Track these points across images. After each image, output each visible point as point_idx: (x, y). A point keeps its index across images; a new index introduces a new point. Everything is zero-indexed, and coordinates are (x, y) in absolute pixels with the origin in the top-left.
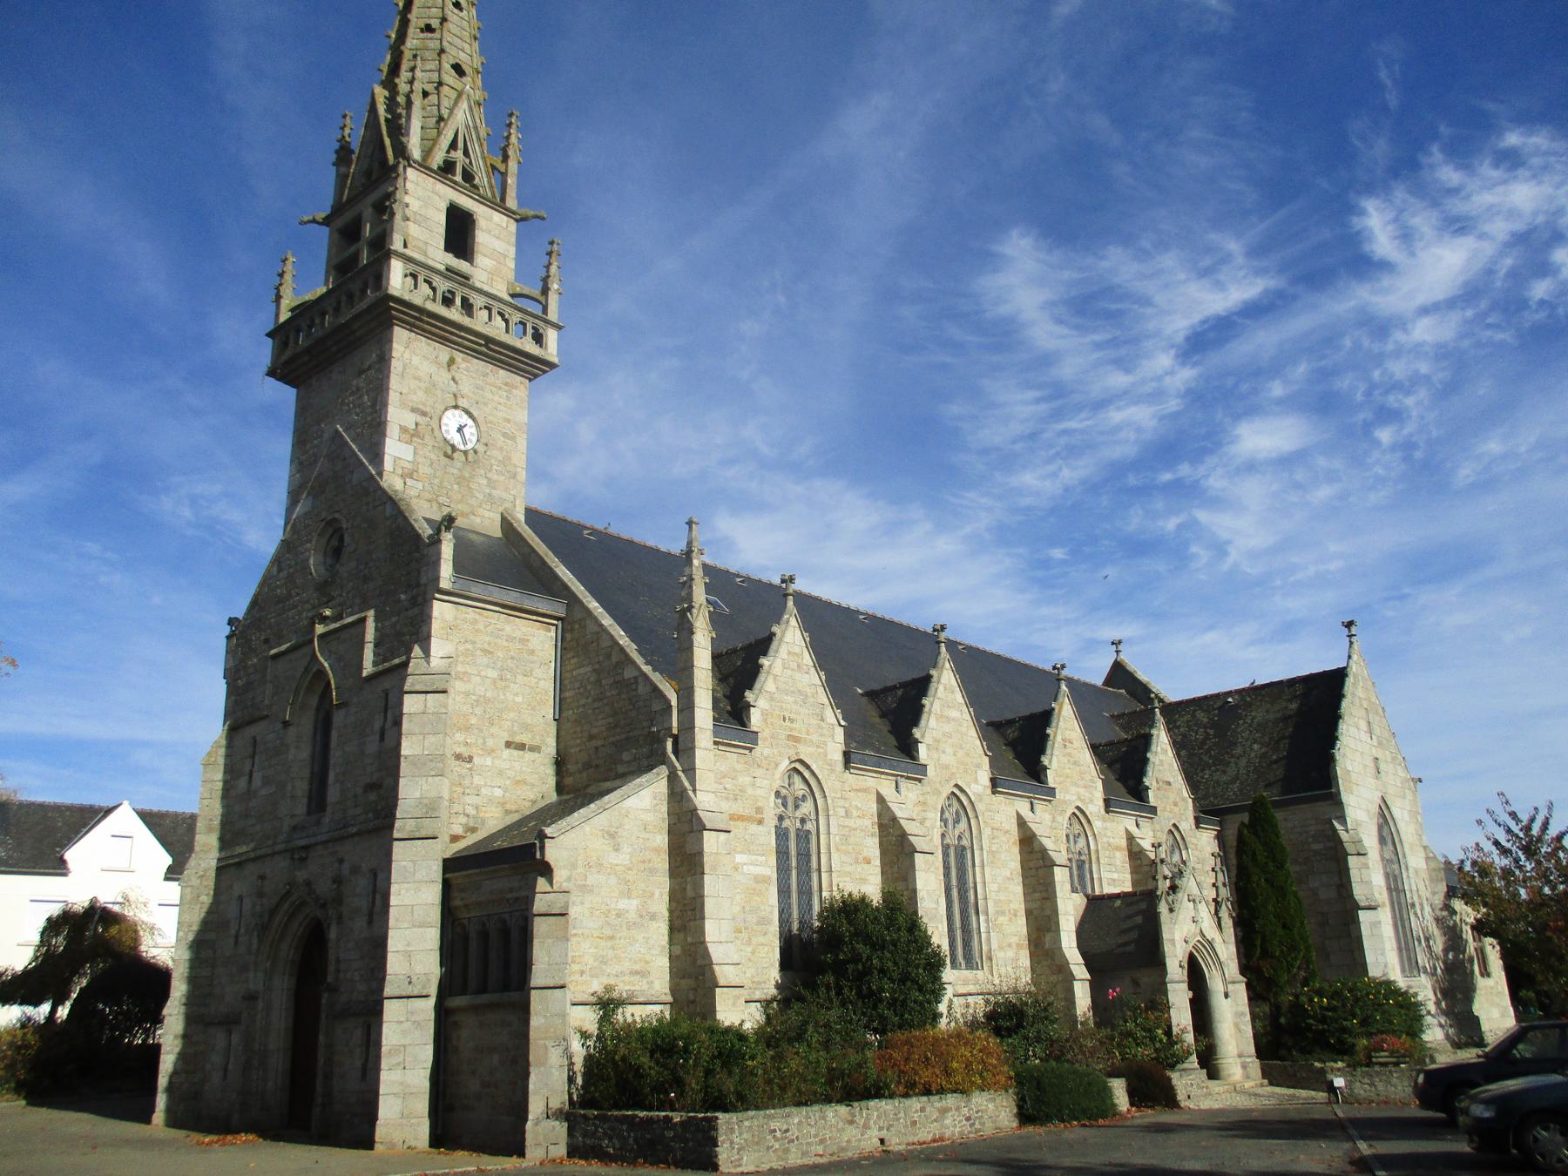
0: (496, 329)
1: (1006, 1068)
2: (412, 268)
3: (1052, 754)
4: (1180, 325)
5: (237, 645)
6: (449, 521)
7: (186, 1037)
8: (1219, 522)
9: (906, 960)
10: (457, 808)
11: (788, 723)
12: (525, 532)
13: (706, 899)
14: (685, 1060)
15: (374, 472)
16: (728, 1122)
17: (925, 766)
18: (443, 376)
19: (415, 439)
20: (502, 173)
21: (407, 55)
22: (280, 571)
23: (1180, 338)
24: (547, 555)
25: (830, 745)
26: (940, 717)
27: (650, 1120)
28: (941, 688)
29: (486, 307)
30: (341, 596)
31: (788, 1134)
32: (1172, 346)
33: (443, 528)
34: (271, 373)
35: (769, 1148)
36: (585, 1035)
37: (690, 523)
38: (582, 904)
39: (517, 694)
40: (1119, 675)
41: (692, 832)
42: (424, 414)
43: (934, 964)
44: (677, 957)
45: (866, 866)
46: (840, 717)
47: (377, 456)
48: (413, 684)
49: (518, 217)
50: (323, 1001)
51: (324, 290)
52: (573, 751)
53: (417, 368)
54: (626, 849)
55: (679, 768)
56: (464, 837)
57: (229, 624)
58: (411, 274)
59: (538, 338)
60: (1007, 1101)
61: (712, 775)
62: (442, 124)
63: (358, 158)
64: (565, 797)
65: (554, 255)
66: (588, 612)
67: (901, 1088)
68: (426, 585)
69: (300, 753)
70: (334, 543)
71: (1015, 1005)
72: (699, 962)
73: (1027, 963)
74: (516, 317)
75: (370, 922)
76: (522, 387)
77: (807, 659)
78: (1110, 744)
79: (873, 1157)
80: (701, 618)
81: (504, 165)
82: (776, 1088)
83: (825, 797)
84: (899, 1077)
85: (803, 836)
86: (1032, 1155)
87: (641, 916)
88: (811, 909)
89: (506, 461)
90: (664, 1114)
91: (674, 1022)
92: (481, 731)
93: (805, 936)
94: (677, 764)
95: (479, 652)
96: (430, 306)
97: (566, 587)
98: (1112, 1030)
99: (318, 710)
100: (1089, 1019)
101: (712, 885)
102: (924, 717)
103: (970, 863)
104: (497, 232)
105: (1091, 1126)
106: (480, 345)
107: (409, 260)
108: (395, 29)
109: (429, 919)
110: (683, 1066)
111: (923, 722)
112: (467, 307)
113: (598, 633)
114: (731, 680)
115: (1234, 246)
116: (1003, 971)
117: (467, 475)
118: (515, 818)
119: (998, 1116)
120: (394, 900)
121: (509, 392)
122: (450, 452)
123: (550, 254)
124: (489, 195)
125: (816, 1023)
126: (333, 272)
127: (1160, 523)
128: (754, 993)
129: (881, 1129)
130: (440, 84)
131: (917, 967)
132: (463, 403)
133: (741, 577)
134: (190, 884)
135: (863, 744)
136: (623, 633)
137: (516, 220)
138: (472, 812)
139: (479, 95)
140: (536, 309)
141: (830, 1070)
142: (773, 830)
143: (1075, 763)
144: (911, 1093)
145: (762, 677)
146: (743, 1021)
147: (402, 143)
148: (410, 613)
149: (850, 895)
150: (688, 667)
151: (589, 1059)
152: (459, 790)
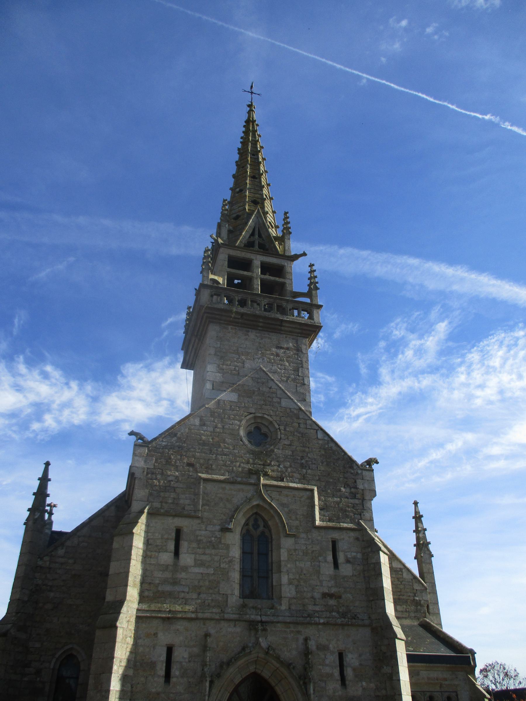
134: (122, 626)
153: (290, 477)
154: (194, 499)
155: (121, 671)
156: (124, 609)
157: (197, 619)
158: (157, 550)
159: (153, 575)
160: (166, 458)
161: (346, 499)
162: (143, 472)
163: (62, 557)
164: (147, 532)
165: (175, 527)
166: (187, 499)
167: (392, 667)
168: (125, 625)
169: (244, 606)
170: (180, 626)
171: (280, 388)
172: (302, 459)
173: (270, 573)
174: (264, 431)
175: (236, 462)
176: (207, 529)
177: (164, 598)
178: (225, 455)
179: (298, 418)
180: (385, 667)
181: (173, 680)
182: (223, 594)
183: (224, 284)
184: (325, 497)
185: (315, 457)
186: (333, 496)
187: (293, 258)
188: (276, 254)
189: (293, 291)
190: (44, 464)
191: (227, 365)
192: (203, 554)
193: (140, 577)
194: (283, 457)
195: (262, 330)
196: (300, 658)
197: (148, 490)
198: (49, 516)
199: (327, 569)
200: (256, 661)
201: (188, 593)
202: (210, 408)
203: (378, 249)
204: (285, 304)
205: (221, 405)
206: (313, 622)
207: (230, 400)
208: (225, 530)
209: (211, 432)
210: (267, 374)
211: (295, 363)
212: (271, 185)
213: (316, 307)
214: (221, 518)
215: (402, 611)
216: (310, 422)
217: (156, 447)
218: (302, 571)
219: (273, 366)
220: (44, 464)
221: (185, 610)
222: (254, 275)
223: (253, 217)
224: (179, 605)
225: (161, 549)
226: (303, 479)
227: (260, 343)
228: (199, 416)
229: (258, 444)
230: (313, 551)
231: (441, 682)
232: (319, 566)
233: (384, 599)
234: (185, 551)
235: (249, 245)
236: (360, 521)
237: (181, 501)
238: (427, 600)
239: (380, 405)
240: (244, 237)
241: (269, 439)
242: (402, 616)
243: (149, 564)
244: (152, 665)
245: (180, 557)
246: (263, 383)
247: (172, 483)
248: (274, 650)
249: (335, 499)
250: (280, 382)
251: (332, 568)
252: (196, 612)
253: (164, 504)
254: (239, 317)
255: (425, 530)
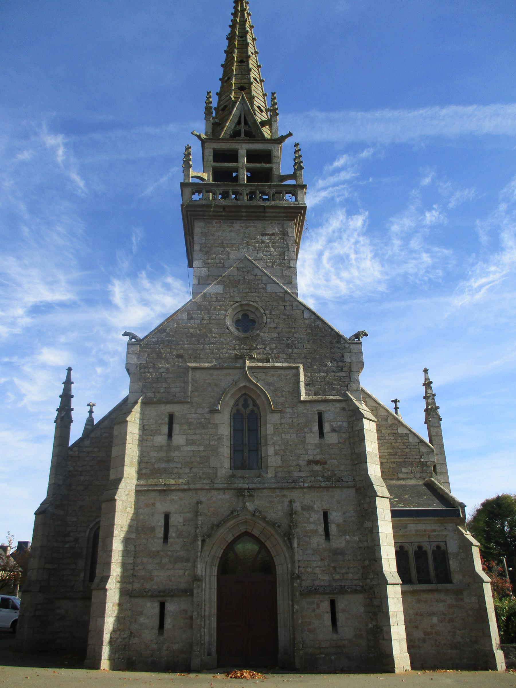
4: (31, 299)
8: (23, 386)
23: (30, 304)
37: (426, 371)
115: (62, 277)
134: (121, 499)
153: (276, 358)
154: (184, 387)
155: (122, 535)
156: (122, 485)
157: (189, 490)
158: (153, 434)
159: (149, 455)
160: (157, 353)
161: (333, 373)
162: (137, 367)
163: (88, 447)
164: (142, 419)
165: (168, 412)
166: (177, 387)
167: (373, 522)
168: (124, 498)
169: (233, 476)
170: (175, 496)
171: (265, 274)
172: (288, 340)
173: (259, 446)
174: (251, 318)
175: (223, 349)
176: (197, 412)
177: (160, 474)
178: (213, 344)
179: (284, 301)
180: (367, 522)
181: (170, 540)
182: (213, 467)
183: (209, 179)
184: (310, 372)
185: (302, 336)
186: (320, 371)
187: (279, 140)
188: (264, 140)
189: (281, 174)
190: (67, 369)
191: (212, 259)
192: (194, 434)
193: (137, 458)
194: (269, 339)
195: (246, 220)
196: (285, 518)
197: (142, 383)
198: (89, 414)
199: (313, 439)
200: (246, 522)
201: (181, 469)
202: (197, 302)
203: (484, 102)
204: (268, 189)
205: (207, 298)
206: (298, 486)
207: (215, 292)
208: (213, 411)
209: (198, 324)
210: (252, 262)
211: (281, 248)
212: (262, 66)
213: (299, 188)
214: (209, 401)
215: (407, 473)
216: (296, 303)
217: (147, 344)
218: (288, 442)
219: (258, 253)
220: (67, 369)
221: (178, 483)
222: (240, 165)
223: (237, 105)
224: (173, 479)
225: (157, 433)
226: (290, 358)
227: (245, 233)
228: (186, 311)
229: (245, 331)
230: (299, 424)
231: (430, 533)
232: (305, 437)
233: (366, 462)
234: (178, 433)
235: (235, 135)
236: (346, 392)
237: (173, 390)
238: (433, 461)
239: (504, 272)
240: (229, 127)
241: (256, 325)
242: (407, 477)
243: (145, 446)
244: (152, 529)
245: (173, 439)
246: (248, 271)
247: (163, 374)
248: (260, 512)
249: (322, 374)
250: (265, 268)
251: (318, 438)
252: (188, 483)
253: (156, 394)
254: (221, 210)
255: (434, 395)
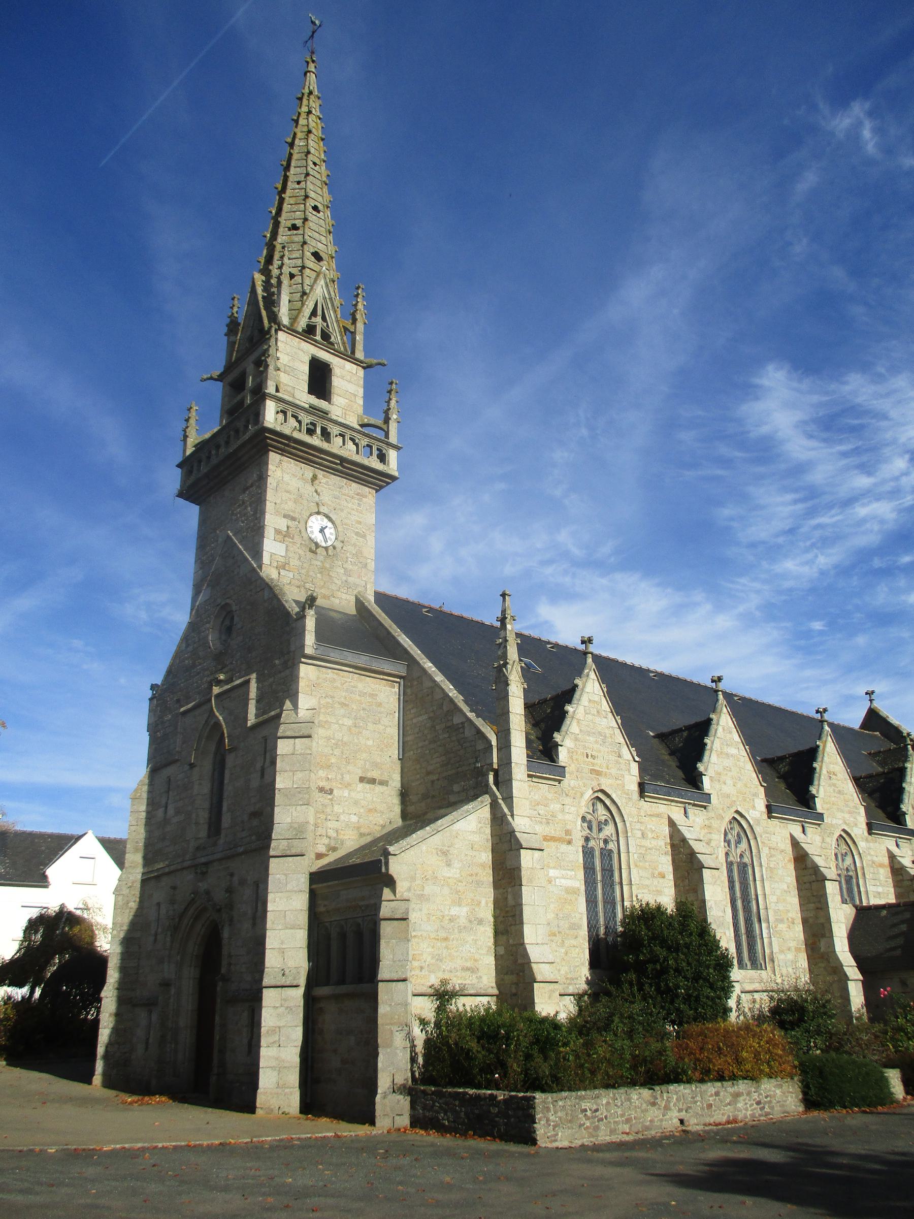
0: (349, 451)
1: (790, 1058)
2: (282, 406)
3: (819, 785)
5: (157, 706)
6: (311, 601)
7: (118, 1015)
9: (698, 961)
10: (320, 831)
11: (590, 759)
12: (374, 609)
13: (524, 908)
14: (508, 1045)
15: (255, 566)
16: (544, 1102)
17: (710, 795)
18: (309, 489)
19: (286, 539)
20: (352, 333)
21: (278, 247)
22: (188, 646)
24: (390, 627)
25: (627, 777)
26: (720, 754)
27: (478, 1097)
28: (720, 729)
29: (340, 435)
30: (232, 663)
31: (597, 1114)
32: (907, 452)
33: (307, 606)
34: (180, 495)
35: (581, 1125)
36: (423, 1022)
37: (504, 595)
38: (421, 910)
39: (368, 739)
40: (874, 719)
41: (511, 850)
42: (293, 519)
43: (723, 965)
44: (502, 956)
45: (661, 880)
46: (635, 754)
47: (257, 553)
48: (284, 731)
49: (365, 365)
50: (218, 989)
51: (219, 428)
52: (414, 784)
53: (288, 484)
54: (456, 864)
55: (499, 796)
56: (327, 855)
57: (151, 689)
58: (282, 411)
59: (382, 458)
60: (793, 1087)
61: (527, 803)
62: (305, 297)
63: (243, 328)
64: (408, 822)
65: (393, 392)
66: (424, 671)
67: (697, 1074)
68: (294, 652)
69: (202, 789)
70: (227, 623)
71: (796, 1001)
72: (520, 961)
73: (805, 964)
74: (364, 442)
75: (254, 924)
76: (370, 496)
77: (605, 706)
78: (870, 776)
79: (674, 1136)
80: (514, 672)
81: (353, 327)
82: (586, 1071)
83: (624, 821)
84: (695, 1064)
85: (607, 855)
86: (818, 1141)
87: (470, 921)
88: (615, 916)
89: (358, 554)
90: (489, 1092)
91: (499, 1012)
92: (339, 768)
93: (610, 939)
94: (498, 794)
95: (336, 705)
96: (296, 435)
97: (405, 650)
98: (885, 1025)
99: (216, 754)
100: (863, 1015)
101: (529, 895)
102: (707, 753)
103: (751, 878)
104: (349, 378)
105: (871, 1113)
106: (336, 464)
107: (280, 400)
108: (270, 230)
109: (299, 923)
110: (506, 1050)
111: (706, 758)
112: (326, 434)
113: (432, 687)
114: (543, 725)
116: (784, 972)
117: (328, 566)
118: (369, 839)
119: (785, 1101)
120: (270, 907)
121: (360, 500)
122: (314, 548)
123: (390, 392)
124: (342, 349)
125: (622, 1016)
126: (226, 416)
127: (903, 598)
128: (568, 988)
129: (680, 1110)
130: (303, 267)
131: (708, 967)
132: (323, 509)
133: (551, 644)
134: (121, 893)
135: (655, 777)
136: (451, 687)
137: (363, 368)
138: (332, 833)
139: (333, 274)
140: (380, 435)
141: (634, 1057)
142: (580, 849)
143: (839, 792)
144: (706, 1078)
145: (567, 721)
146: (557, 1012)
147: (274, 312)
148: (283, 674)
149: (648, 904)
150: (506, 713)
151: (428, 1042)
152: (323, 816)
